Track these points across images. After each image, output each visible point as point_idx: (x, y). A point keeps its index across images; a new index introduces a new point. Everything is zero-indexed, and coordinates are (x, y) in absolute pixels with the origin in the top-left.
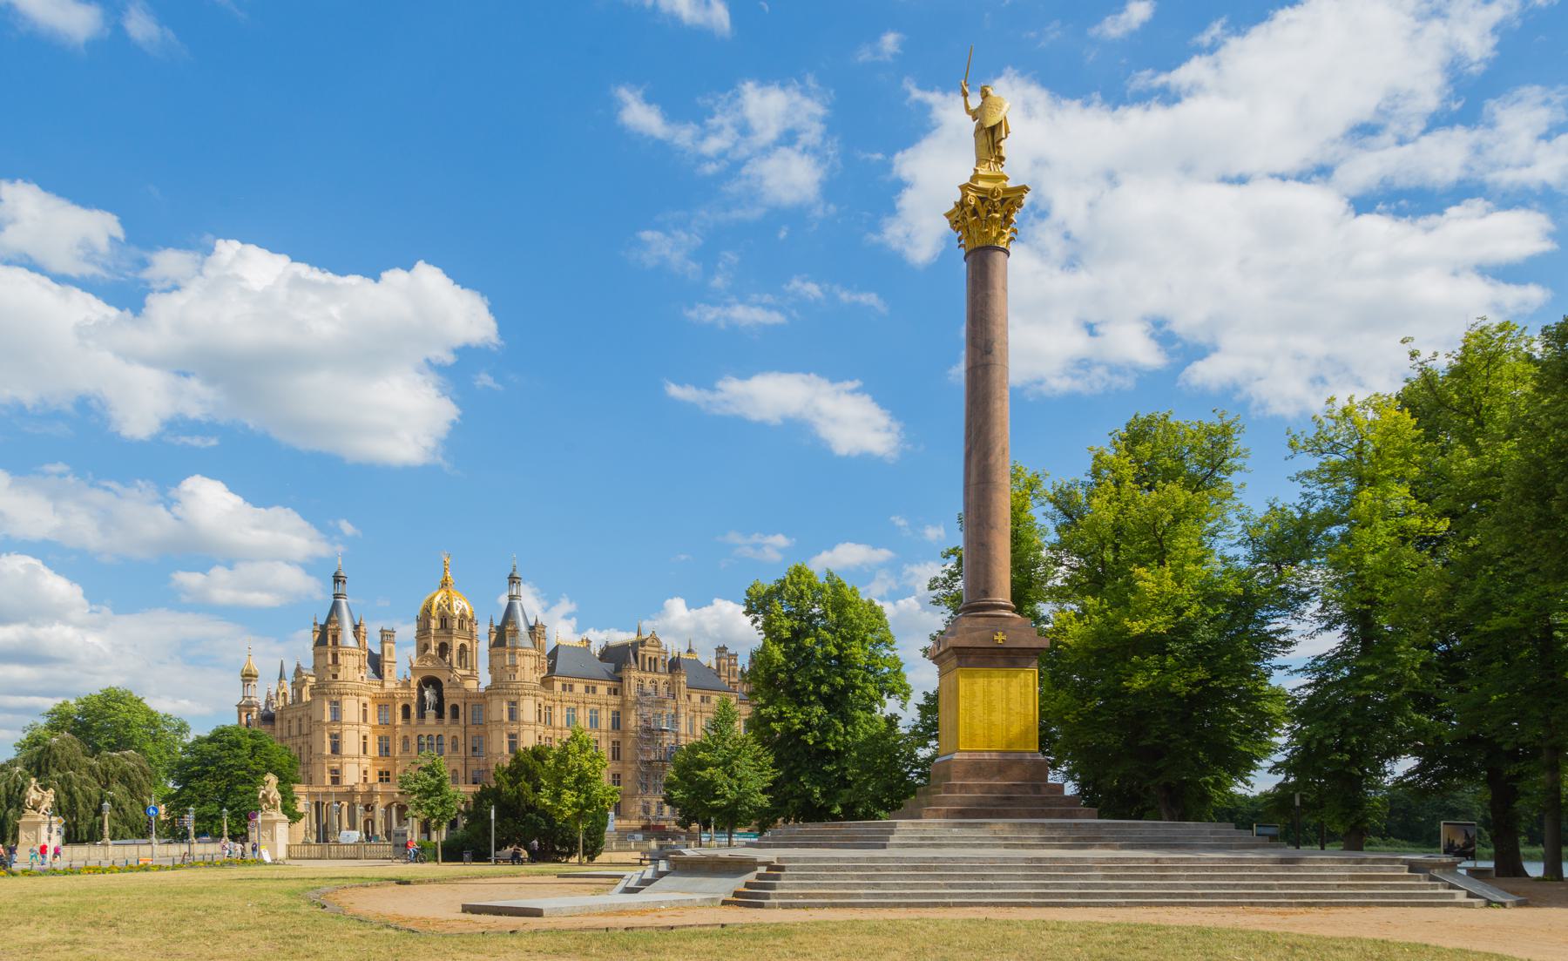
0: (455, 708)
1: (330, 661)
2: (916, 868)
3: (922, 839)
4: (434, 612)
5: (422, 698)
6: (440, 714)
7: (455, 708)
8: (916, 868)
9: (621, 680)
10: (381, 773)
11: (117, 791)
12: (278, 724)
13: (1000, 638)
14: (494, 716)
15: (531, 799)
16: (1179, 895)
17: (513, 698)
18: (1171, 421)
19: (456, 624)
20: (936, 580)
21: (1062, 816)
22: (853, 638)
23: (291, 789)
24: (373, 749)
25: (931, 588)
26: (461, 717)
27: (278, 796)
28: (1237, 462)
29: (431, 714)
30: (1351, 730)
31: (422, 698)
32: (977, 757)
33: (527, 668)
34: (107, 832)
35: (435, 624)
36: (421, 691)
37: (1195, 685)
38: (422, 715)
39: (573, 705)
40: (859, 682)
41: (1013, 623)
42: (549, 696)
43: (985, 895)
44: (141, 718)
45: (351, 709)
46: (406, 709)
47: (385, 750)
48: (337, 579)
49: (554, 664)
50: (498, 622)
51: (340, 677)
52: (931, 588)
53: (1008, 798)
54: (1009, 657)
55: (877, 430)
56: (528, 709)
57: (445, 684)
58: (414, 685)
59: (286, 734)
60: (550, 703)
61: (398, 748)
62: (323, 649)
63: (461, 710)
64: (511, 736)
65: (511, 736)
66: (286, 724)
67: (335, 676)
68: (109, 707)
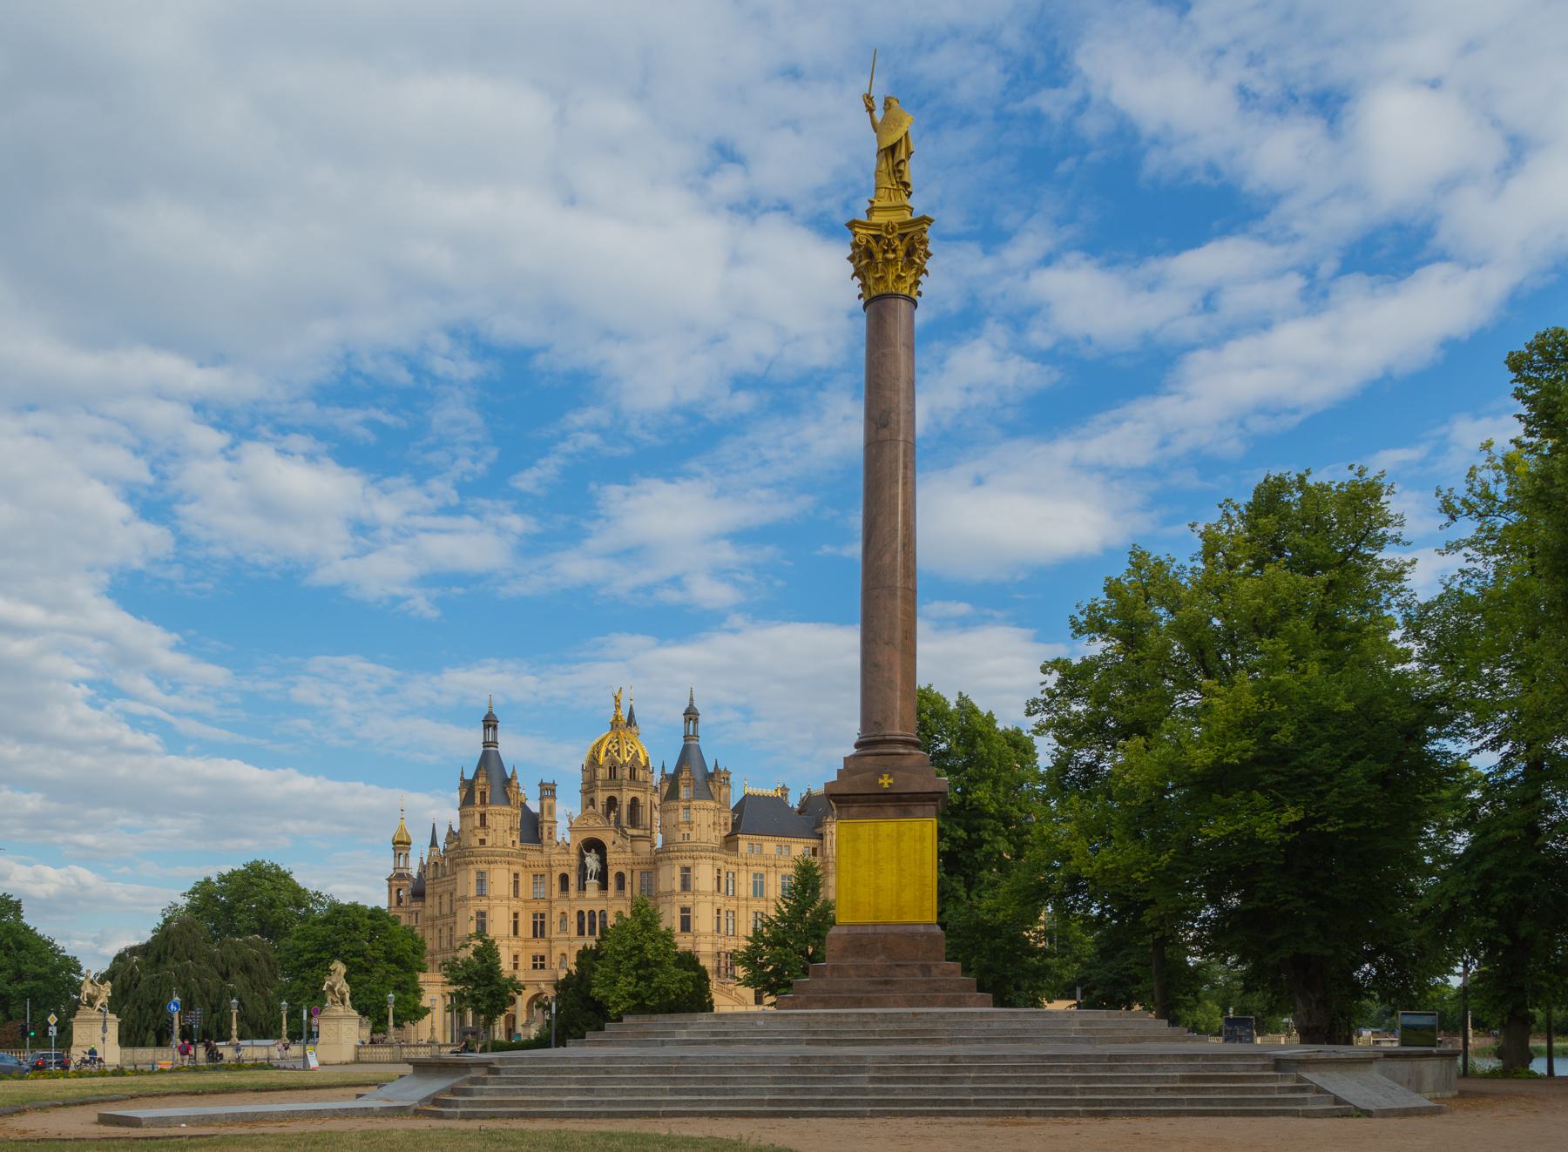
0: (620, 877)
1: (478, 823)
2: (652, 1070)
3: (714, 1034)
4: (602, 758)
5: (583, 867)
6: (604, 886)
7: (620, 877)
8: (652, 1070)
9: (821, 837)
10: (535, 959)
11: (237, 982)
12: (429, 901)
13: (886, 781)
14: (663, 887)
15: (1539, 1014)
16: (945, 1103)
17: (688, 863)
18: (1311, 481)
19: (627, 772)
20: (1035, 702)
21: (948, 1004)
22: (983, 778)
23: (415, 979)
24: (526, 928)
25: (1029, 713)
26: (628, 887)
27: (346, 988)
28: (1391, 531)
29: (592, 884)
30: (1496, 886)
31: (583, 867)
32: (859, 930)
33: (704, 825)
34: (234, 1033)
35: (602, 773)
36: (582, 857)
37: (1287, 829)
38: (582, 887)
39: (762, 870)
40: (986, 835)
41: (908, 762)
42: (733, 859)
43: (710, 1102)
44: (285, 896)
45: (500, 880)
46: (564, 879)
47: (539, 929)
48: (490, 723)
49: (740, 818)
50: (670, 770)
51: (489, 843)
52: (1029, 713)
53: (886, 982)
54: (901, 803)
55: (1383, 474)
56: (704, 876)
57: (610, 848)
58: (574, 849)
59: (437, 913)
60: (733, 868)
61: (556, 927)
62: (470, 809)
63: (628, 880)
64: (685, 910)
65: (685, 910)
66: (437, 900)
67: (483, 842)
68: (252, 884)
